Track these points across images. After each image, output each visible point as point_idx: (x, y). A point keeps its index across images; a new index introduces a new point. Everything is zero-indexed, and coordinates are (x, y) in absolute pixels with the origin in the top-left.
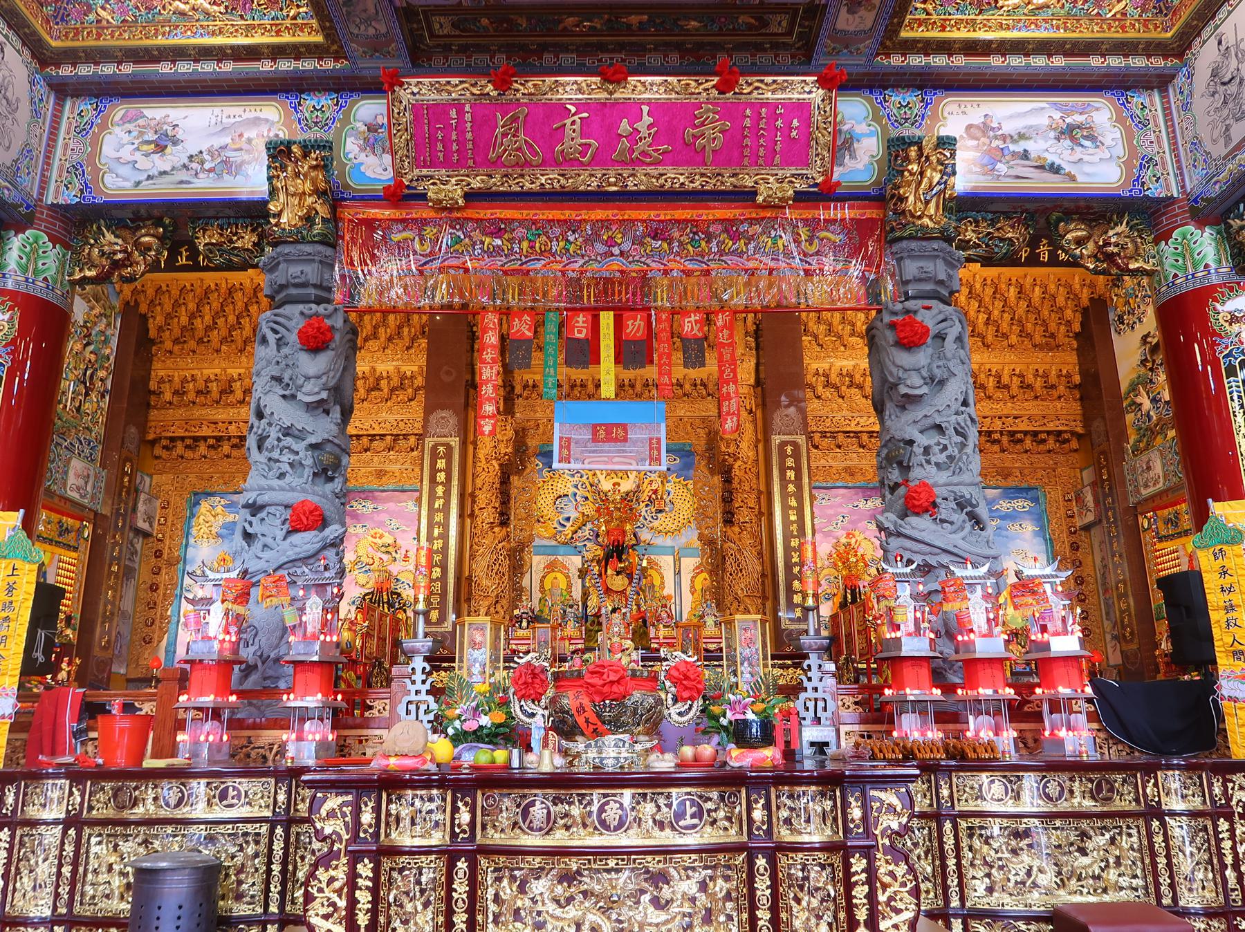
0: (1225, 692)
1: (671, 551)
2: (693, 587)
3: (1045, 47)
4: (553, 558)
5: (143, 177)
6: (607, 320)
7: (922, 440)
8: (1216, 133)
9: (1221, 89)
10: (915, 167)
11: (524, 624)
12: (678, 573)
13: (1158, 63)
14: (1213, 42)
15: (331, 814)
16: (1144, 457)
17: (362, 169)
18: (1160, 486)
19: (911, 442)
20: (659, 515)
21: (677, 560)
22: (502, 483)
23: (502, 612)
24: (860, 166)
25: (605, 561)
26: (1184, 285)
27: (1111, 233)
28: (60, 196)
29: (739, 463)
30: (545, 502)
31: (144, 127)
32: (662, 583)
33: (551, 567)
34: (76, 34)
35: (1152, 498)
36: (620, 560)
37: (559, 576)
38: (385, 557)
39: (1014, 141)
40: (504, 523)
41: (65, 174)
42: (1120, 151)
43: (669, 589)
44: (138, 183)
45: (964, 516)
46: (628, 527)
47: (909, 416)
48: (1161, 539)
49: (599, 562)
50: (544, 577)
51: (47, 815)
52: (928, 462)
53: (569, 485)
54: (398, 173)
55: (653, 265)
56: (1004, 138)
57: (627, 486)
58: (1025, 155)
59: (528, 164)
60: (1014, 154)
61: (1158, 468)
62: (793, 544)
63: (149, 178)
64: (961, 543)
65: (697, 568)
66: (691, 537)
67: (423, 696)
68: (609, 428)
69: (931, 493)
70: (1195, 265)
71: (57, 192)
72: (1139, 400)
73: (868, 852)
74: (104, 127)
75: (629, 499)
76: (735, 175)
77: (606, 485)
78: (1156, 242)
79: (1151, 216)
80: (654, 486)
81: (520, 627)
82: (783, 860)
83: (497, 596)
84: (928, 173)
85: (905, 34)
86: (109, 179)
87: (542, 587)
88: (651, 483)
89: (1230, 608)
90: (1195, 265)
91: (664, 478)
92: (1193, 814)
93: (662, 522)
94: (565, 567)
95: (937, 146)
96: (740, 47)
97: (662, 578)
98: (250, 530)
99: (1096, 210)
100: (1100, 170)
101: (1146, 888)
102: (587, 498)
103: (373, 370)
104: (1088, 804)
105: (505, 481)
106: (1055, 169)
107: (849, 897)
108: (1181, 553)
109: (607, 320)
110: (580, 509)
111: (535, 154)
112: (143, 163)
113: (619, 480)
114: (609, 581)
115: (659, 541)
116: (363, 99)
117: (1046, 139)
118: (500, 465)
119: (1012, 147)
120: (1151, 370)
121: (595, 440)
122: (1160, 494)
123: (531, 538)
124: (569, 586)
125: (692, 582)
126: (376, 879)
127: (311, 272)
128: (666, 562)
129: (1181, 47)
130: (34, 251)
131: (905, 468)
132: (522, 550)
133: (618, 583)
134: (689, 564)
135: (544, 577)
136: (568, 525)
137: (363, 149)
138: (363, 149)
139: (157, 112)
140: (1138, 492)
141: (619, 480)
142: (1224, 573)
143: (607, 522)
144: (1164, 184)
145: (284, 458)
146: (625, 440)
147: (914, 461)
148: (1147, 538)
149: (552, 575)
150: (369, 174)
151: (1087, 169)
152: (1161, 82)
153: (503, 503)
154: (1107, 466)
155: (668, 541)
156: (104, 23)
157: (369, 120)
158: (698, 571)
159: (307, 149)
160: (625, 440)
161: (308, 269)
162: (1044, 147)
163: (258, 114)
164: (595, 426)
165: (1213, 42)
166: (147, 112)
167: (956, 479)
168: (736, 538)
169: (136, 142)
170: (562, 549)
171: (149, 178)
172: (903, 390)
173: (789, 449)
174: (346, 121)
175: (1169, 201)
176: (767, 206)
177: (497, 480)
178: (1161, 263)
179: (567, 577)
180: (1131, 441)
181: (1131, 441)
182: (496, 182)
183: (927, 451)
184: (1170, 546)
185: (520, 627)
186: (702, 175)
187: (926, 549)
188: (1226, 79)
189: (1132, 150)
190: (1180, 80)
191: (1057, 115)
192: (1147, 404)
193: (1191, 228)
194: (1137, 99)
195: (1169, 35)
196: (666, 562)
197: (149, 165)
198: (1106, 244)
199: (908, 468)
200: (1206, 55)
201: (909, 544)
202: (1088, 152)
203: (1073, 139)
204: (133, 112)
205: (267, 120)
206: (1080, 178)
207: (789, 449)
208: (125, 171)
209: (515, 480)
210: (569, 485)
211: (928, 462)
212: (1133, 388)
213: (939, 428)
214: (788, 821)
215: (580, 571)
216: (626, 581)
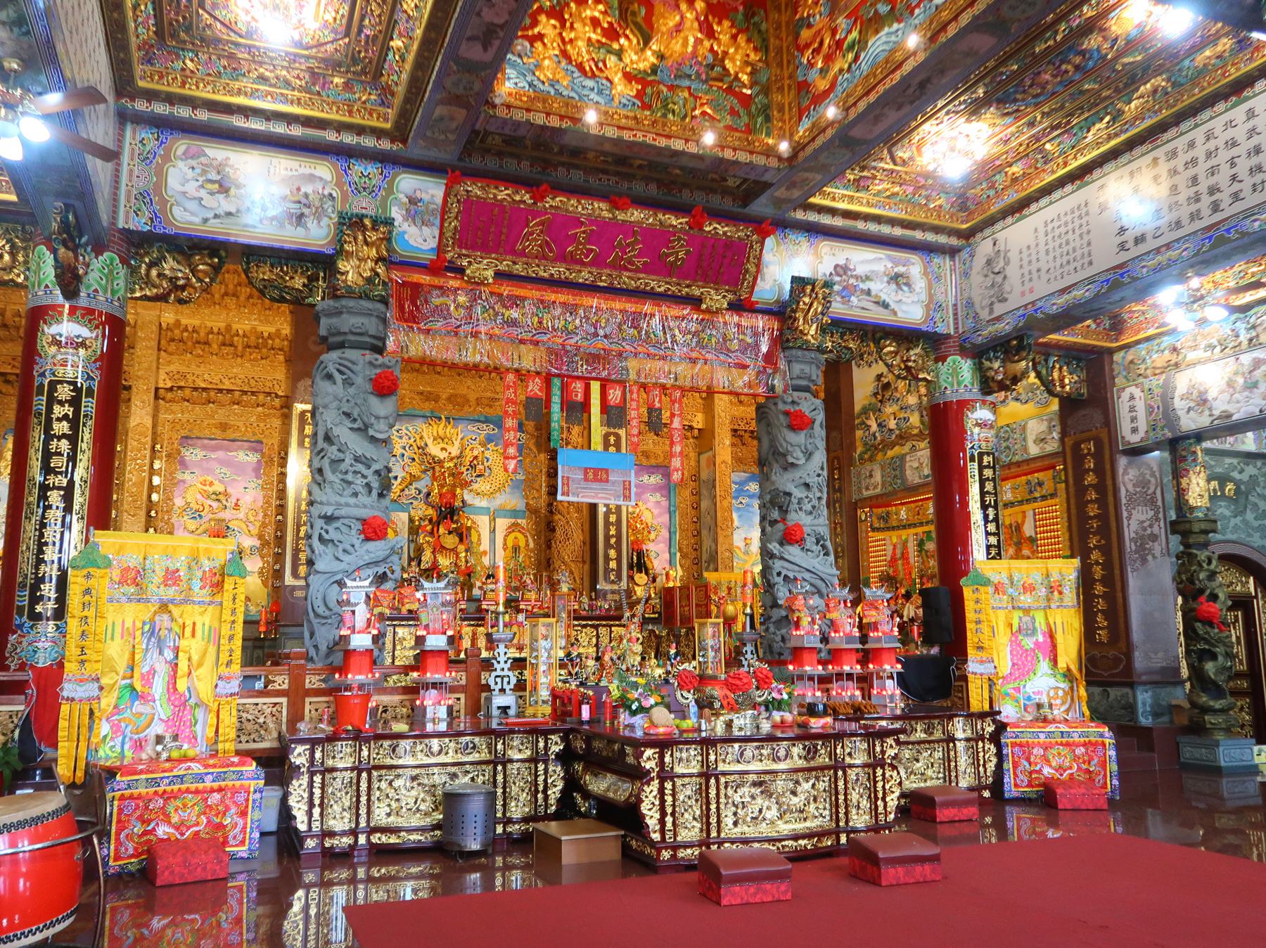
0: (970, 669)
3: (892, 222)
5: (210, 215)
6: (595, 387)
7: (798, 493)
8: (984, 303)
9: (992, 276)
10: (807, 300)
12: (493, 531)
13: (954, 241)
14: (989, 242)
15: (649, 759)
16: (868, 466)
17: (406, 237)
18: (878, 491)
19: (789, 494)
21: (493, 520)
24: (768, 287)
26: (951, 396)
27: (912, 352)
28: (131, 221)
31: (206, 165)
32: (479, 540)
34: (161, 77)
35: (871, 498)
38: (215, 504)
39: (863, 281)
41: (133, 200)
42: (924, 297)
43: (485, 545)
44: (206, 220)
45: (819, 548)
47: (789, 475)
48: (873, 530)
49: (430, 521)
51: (340, 765)
52: (801, 509)
54: (440, 249)
55: (627, 347)
56: (857, 277)
57: (455, 451)
58: (868, 292)
59: (545, 258)
60: (862, 291)
61: (878, 477)
63: (216, 216)
64: (818, 566)
67: (506, 672)
68: (596, 471)
69: (802, 533)
70: (959, 384)
71: (127, 217)
72: (869, 423)
73: (546, 762)
74: (167, 158)
76: (688, 286)
77: (435, 450)
78: (936, 360)
79: (935, 344)
80: (475, 453)
84: (815, 305)
85: (812, 200)
86: (177, 211)
88: (472, 450)
89: (978, 622)
90: (959, 384)
92: (968, 740)
93: (481, 485)
95: (823, 286)
96: (700, 188)
98: (327, 537)
99: (906, 336)
100: (910, 310)
101: (944, 778)
102: (414, 459)
103: (229, 328)
104: (923, 735)
106: (885, 305)
107: (875, 787)
108: (888, 542)
109: (595, 387)
110: (407, 469)
111: (551, 250)
112: (208, 201)
116: (404, 172)
117: (882, 282)
119: (862, 286)
120: (881, 401)
121: (586, 479)
122: (877, 496)
125: (505, 540)
126: (673, 789)
127: (371, 325)
129: (968, 235)
130: (111, 271)
131: (784, 511)
133: (450, 541)
134: (502, 524)
137: (406, 219)
138: (406, 219)
139: (217, 152)
140: (860, 491)
142: (977, 602)
144: (945, 326)
145: (358, 482)
146: (607, 481)
147: (792, 507)
148: (862, 527)
150: (412, 242)
151: (904, 308)
152: (953, 252)
154: (839, 469)
156: (188, 72)
157: (410, 193)
158: (513, 528)
159: (376, 223)
160: (607, 481)
161: (365, 320)
162: (879, 288)
163: (313, 171)
164: (586, 469)
165: (989, 242)
166: (208, 151)
167: (816, 522)
169: (201, 179)
171: (216, 216)
172: (791, 460)
173: (612, 439)
174: (390, 191)
175: (948, 336)
176: (708, 311)
178: (937, 377)
180: (858, 452)
181: (858, 452)
182: (519, 269)
183: (800, 501)
184: (880, 536)
186: (667, 283)
187: (797, 568)
189: (931, 296)
190: (964, 254)
191: (890, 265)
192: (874, 427)
193: (959, 358)
194: (937, 260)
195: (965, 226)
196: (483, 522)
197: (214, 205)
198: (908, 360)
199: (786, 511)
200: (984, 247)
201: (786, 565)
202: (905, 295)
203: (898, 284)
204: (194, 150)
205: (321, 179)
206: (899, 314)
207: (612, 439)
208: (192, 206)
211: (801, 509)
212: (865, 411)
213: (807, 485)
214: (850, 754)
216: (457, 539)
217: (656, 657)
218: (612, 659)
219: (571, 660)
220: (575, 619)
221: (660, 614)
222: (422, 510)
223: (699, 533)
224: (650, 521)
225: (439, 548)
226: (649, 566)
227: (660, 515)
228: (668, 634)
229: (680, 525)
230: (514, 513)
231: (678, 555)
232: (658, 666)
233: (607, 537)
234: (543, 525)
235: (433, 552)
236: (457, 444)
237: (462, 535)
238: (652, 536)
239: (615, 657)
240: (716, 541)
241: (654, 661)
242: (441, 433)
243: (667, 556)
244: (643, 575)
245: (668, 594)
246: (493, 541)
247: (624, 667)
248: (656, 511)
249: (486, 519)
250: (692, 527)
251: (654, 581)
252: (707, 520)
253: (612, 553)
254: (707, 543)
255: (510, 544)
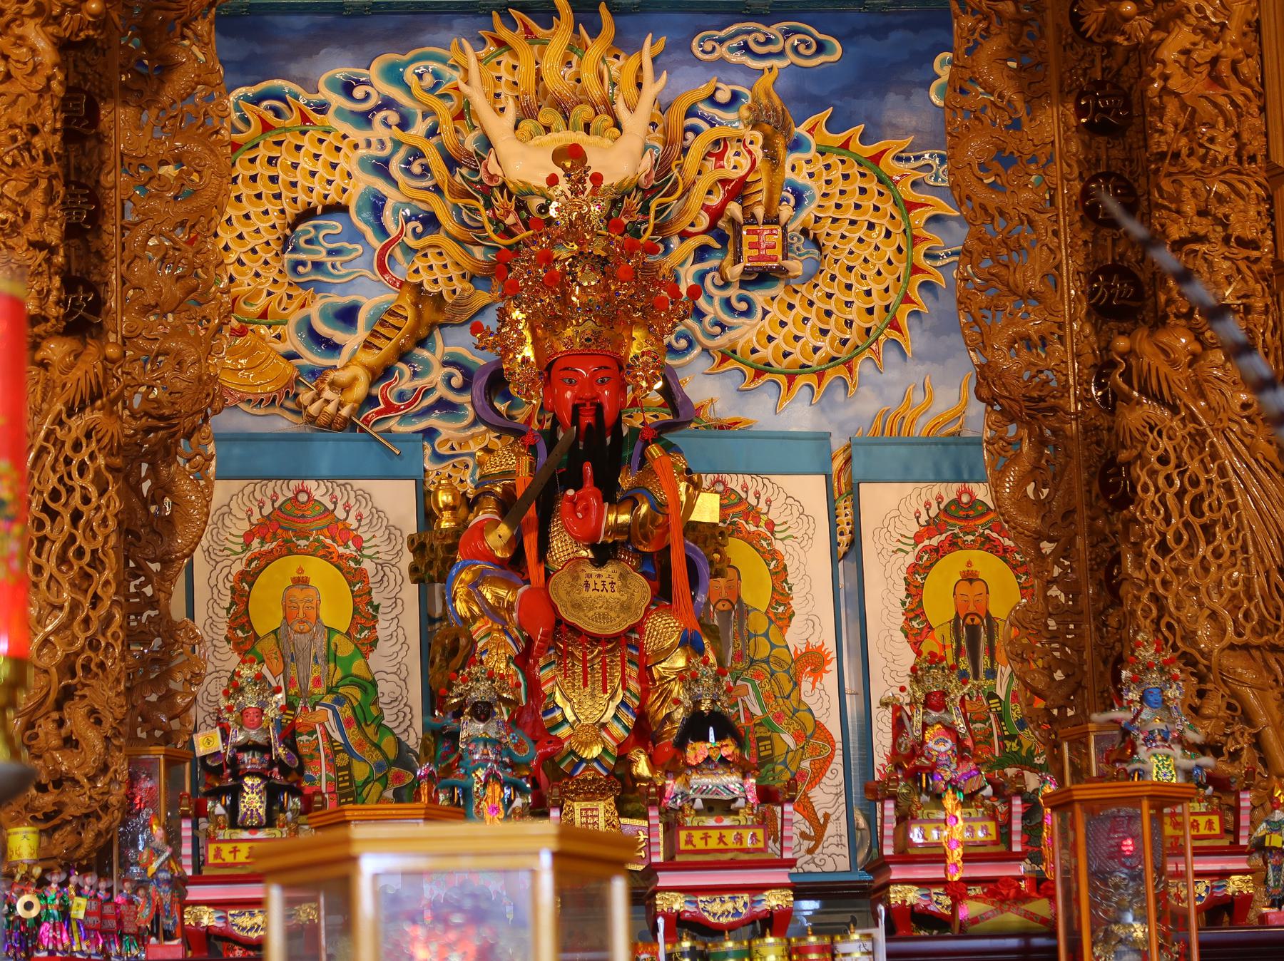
1: (809, 452)
2: (915, 610)
4: (285, 491)
11: (253, 801)
12: (848, 552)
20: (759, 296)
21: (844, 495)
22: (70, 136)
23: (92, 737)
25: (534, 508)
29: (1182, 36)
30: (244, 239)
32: (781, 595)
33: (281, 531)
36: (610, 495)
37: (317, 570)
40: (82, 323)
43: (813, 622)
46: (637, 344)
49: (507, 506)
50: (249, 577)
53: (348, 161)
57: (619, 159)
65: (932, 527)
66: (935, 389)
75: (637, 215)
77: (525, 161)
80: (735, 165)
81: (234, 820)
83: (68, 668)
87: (240, 619)
88: (718, 149)
91: (777, 132)
94: (342, 533)
97: (780, 574)
102: (431, 222)
105: (81, 126)
110: (402, 268)
113: (579, 137)
114: (560, 591)
115: (766, 411)
118: (64, 46)
123: (210, 396)
124: (365, 615)
125: (914, 591)
128: (797, 501)
132: (166, 453)
133: (604, 596)
134: (894, 509)
135: (249, 577)
136: (352, 340)
141: (579, 137)
143: (546, 324)
149: (284, 570)
153: (72, 232)
155: (799, 415)
158: (945, 531)
168: (1179, 379)
170: (327, 451)
177: (50, 118)
179: (355, 576)
185: (234, 820)
188: (21, 99)
196: (797, 501)
209: (122, 125)
210: (348, 161)
215: (418, 546)
216: (641, 589)
222: (472, 453)
225: (553, 638)
230: (947, 454)
234: (1078, 477)
235: (523, 660)
236: (636, 123)
237: (677, 564)
242: (557, 80)
246: (851, 601)
249: (809, 491)
255: (940, 609)
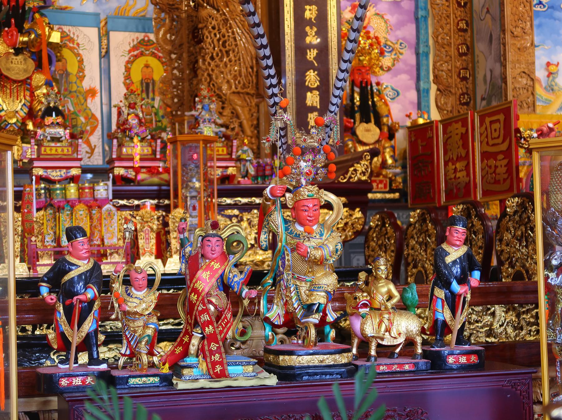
2: (128, 77)
12: (105, 55)
21: (104, 35)
32: (81, 69)
36: (21, 30)
43: (92, 79)
62: (307, 15)
65: (135, 48)
82: (26, 223)
97: (81, 62)
125: (128, 70)
128: (87, 37)
134: (122, 41)
149: (141, 62)
158: (140, 49)
196: (87, 37)
216: (31, 64)
217: (396, 277)
218: (225, 286)
219: (66, 292)
220: (222, 194)
221: (403, 194)
223: (470, 49)
224: (382, 36)
226: (383, 110)
227: (400, 25)
228: (422, 219)
229: (436, 37)
231: (434, 88)
232: (403, 307)
233: (301, 49)
234: (185, 32)
238: (387, 61)
239: (237, 278)
240: (502, 60)
241: (385, 289)
243: (413, 95)
244: (372, 126)
245: (420, 134)
246: (106, 72)
247: (276, 313)
248: (392, 19)
249: (92, 33)
250: (456, 39)
251: (391, 136)
252: (485, 24)
253: (312, 78)
254: (485, 65)
255: (137, 77)
